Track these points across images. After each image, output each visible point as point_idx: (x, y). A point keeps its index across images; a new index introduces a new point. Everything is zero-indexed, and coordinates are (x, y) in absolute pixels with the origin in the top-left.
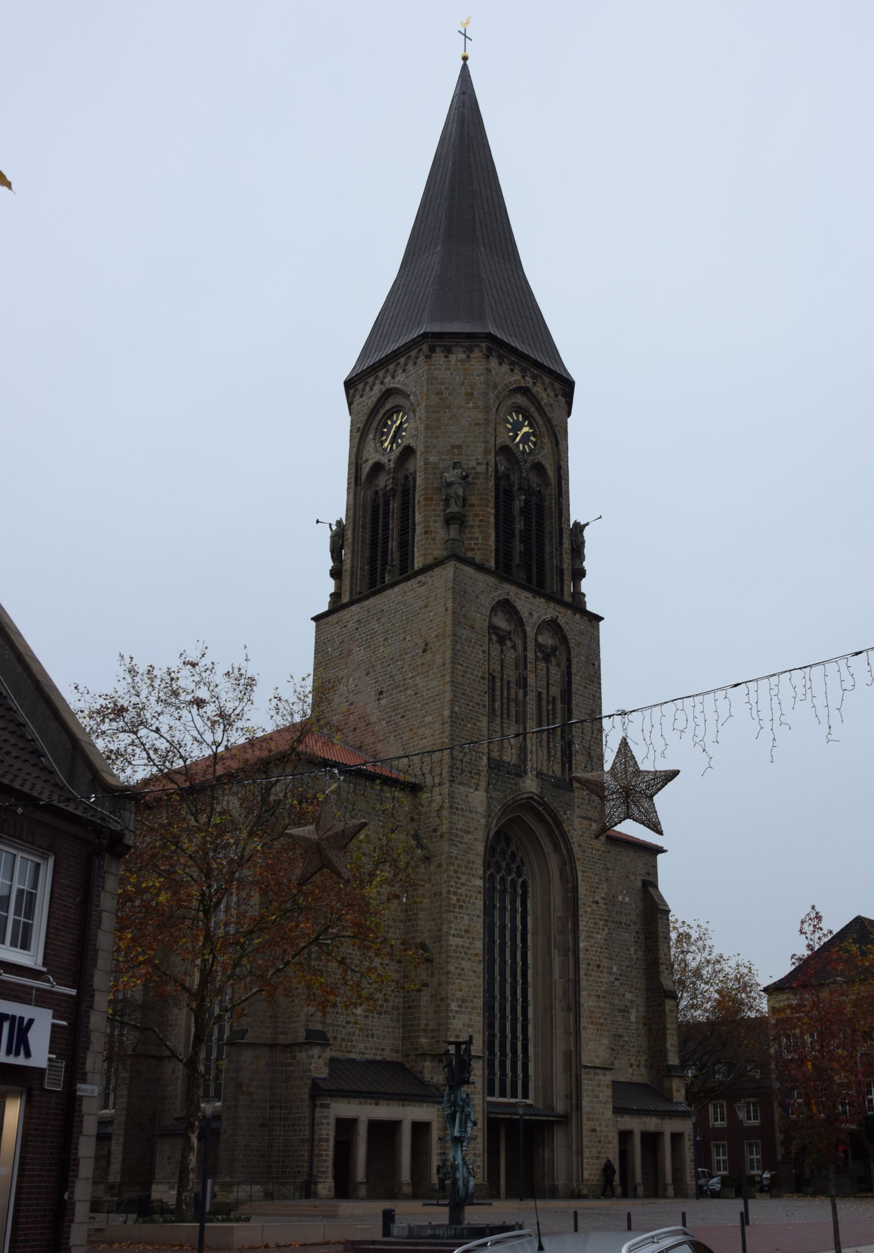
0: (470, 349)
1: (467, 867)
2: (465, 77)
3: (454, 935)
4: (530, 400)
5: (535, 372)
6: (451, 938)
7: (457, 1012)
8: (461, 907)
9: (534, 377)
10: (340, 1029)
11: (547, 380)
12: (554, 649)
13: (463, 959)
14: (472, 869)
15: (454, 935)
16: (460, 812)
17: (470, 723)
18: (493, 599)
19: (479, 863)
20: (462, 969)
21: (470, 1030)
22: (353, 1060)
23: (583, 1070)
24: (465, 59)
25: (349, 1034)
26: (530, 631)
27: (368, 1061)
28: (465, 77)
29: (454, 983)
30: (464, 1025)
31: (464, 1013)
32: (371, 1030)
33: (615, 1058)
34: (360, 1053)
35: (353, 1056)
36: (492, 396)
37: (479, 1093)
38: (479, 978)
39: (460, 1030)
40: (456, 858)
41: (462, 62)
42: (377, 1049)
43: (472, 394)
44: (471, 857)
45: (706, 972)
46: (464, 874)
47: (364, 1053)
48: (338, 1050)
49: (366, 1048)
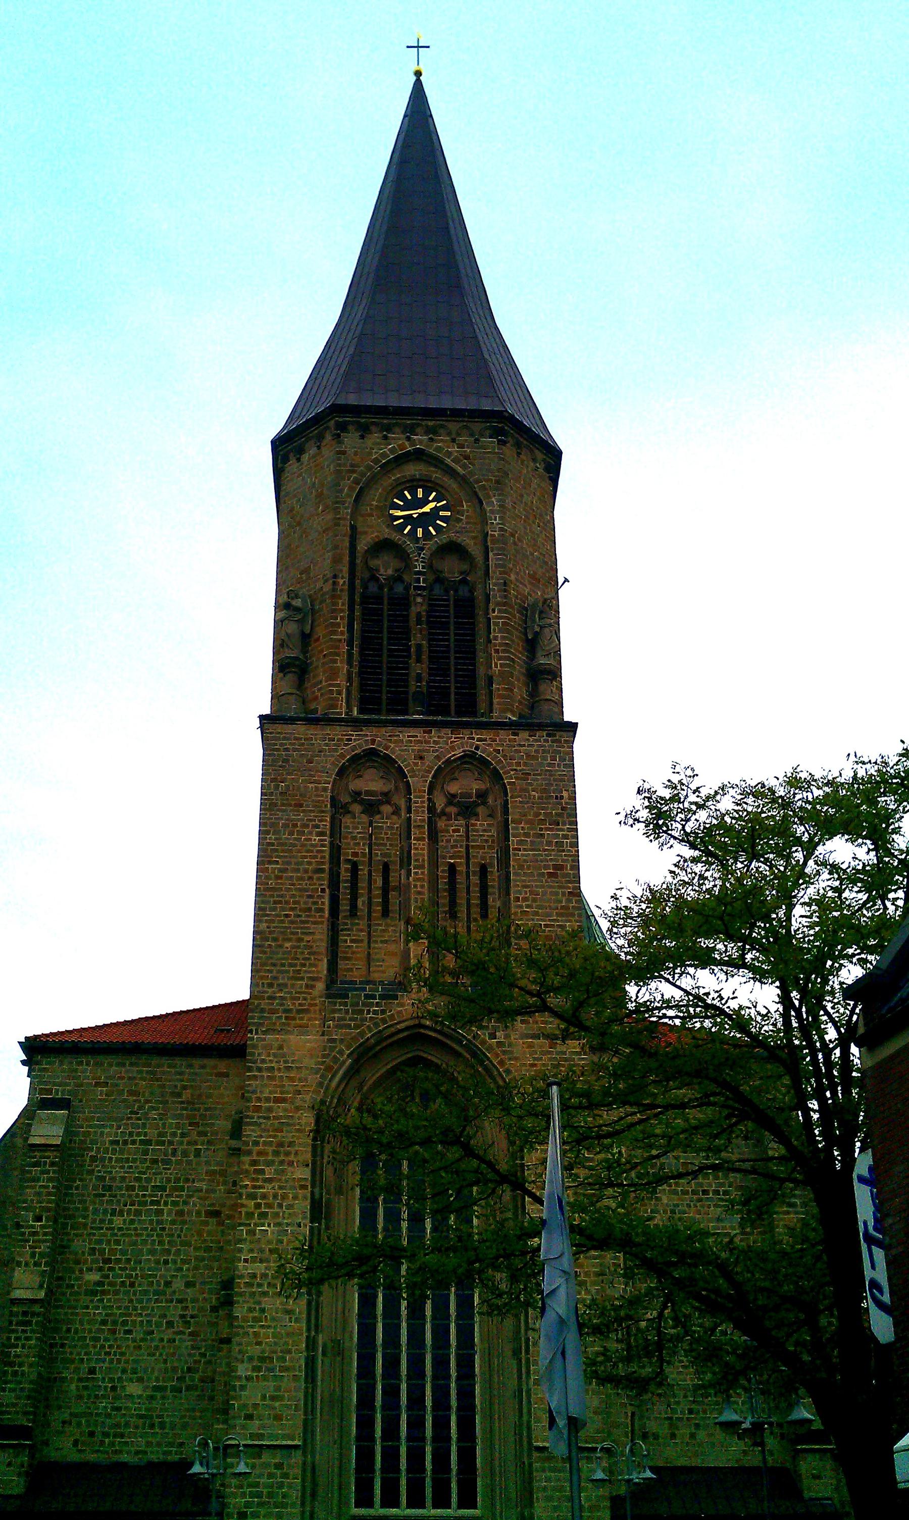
0: (320, 437)
1: (276, 1153)
2: (418, 97)
3: (246, 1261)
4: (430, 464)
5: (430, 423)
6: (241, 1265)
7: (248, 1379)
8: (263, 1215)
9: (428, 431)
10: (100, 1419)
11: (453, 426)
12: (482, 795)
13: (265, 1294)
14: (287, 1154)
15: (246, 1261)
16: (265, 1074)
17: (289, 940)
18: (342, 756)
19: (304, 1147)
20: (263, 1310)
21: (277, 1404)
22: (124, 1465)
23: (535, 1454)
24: (418, 74)
25: (117, 1425)
26: (419, 783)
27: (151, 1464)
28: (418, 97)
29: (247, 1334)
30: (264, 1397)
31: (265, 1378)
32: (159, 1417)
33: (697, 1426)
34: (137, 1453)
35: (125, 1458)
36: (346, 484)
37: (293, 1505)
38: (297, 1320)
39: (256, 1406)
40: (256, 1143)
41: (414, 78)
42: (171, 1444)
43: (322, 493)
44: (287, 1136)
45: (440, 1270)
46: (269, 1164)
47: (146, 1453)
48: (98, 1451)
49: (149, 1444)
